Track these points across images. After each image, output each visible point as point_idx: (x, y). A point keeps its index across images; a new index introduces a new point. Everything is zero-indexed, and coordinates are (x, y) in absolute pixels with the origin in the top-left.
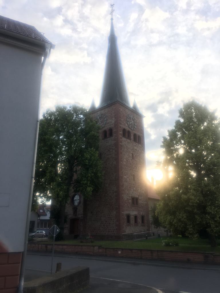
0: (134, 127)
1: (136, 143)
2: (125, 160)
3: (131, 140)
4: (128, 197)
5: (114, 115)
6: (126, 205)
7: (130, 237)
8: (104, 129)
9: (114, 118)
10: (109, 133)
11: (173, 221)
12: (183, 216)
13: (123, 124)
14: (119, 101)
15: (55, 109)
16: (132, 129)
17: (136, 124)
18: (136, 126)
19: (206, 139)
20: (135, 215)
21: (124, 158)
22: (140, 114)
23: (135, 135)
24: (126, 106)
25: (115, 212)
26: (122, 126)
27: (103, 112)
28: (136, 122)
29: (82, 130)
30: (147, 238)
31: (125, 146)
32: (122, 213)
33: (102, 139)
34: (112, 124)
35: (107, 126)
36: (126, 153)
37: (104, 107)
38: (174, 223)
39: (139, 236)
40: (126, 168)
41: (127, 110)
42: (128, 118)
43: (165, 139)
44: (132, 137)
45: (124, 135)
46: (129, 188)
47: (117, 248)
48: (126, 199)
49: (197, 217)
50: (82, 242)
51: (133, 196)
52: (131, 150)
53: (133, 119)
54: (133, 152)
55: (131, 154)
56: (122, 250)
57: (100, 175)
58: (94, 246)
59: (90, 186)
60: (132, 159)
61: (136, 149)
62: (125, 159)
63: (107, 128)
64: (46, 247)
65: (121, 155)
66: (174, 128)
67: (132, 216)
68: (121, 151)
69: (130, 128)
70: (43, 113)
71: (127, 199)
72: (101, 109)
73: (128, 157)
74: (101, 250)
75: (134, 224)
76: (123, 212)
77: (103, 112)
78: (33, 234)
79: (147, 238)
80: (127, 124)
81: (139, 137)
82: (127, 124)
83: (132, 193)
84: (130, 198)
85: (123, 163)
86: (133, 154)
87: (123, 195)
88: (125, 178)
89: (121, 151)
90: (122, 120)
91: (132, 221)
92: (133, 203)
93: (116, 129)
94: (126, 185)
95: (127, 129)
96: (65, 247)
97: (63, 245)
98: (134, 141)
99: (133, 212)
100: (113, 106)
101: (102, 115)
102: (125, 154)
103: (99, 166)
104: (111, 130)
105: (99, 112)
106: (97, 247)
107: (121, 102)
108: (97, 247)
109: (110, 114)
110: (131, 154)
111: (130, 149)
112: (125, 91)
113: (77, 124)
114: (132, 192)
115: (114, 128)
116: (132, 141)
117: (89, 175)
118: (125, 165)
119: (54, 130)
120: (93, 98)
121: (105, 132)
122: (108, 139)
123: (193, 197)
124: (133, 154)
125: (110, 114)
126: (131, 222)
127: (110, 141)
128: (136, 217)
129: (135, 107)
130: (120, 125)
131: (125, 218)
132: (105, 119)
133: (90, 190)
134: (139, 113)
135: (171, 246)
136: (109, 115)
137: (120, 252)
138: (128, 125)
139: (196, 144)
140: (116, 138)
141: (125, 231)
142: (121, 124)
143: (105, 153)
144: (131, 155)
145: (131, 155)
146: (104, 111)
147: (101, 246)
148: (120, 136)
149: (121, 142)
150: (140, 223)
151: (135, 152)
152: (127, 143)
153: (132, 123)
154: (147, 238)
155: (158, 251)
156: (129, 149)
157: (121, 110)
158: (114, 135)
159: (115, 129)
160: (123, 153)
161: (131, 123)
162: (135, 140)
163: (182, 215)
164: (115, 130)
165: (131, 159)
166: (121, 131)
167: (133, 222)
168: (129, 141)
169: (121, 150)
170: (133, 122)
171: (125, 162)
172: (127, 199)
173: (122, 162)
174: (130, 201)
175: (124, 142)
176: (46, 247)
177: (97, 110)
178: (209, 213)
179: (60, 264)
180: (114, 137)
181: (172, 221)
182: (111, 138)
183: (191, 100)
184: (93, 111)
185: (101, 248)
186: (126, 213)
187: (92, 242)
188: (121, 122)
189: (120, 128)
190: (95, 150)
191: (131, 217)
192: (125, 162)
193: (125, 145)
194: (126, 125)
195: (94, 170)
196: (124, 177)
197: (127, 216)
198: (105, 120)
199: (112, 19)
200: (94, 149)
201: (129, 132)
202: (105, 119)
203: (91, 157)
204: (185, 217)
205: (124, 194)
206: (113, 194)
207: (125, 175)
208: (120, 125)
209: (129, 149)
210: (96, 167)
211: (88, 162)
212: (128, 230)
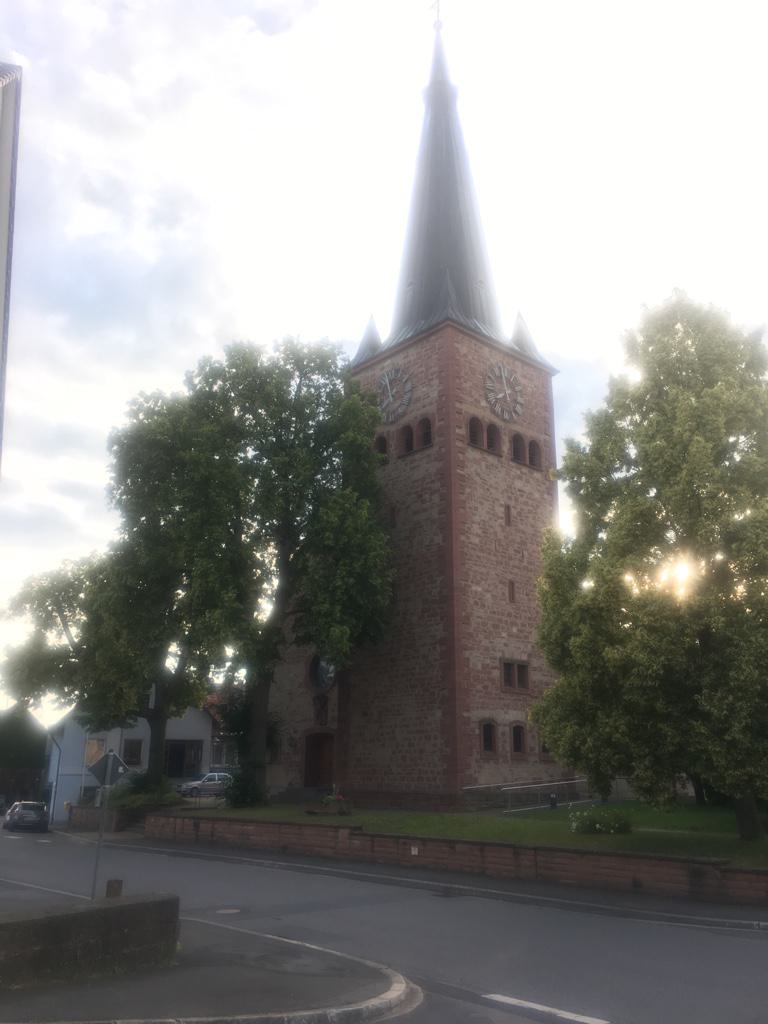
0: (516, 412)
1: (520, 469)
2: (476, 529)
3: (501, 456)
4: (488, 661)
5: (436, 369)
6: (479, 687)
7: (492, 800)
8: (403, 422)
9: (436, 382)
10: (419, 436)
11: (584, 742)
12: (617, 723)
13: (470, 400)
14: (453, 321)
15: (225, 358)
16: (506, 416)
17: (519, 399)
18: (521, 405)
19: (698, 442)
20: (515, 722)
21: (473, 523)
22: (540, 363)
23: (517, 439)
24: (484, 336)
25: (439, 714)
26: (464, 407)
27: (400, 360)
28: (520, 391)
29: (320, 426)
30: (553, 803)
31: (477, 479)
32: (465, 714)
33: (399, 458)
34: (431, 404)
35: (413, 411)
36: (482, 504)
37: (405, 341)
38: (583, 749)
39: (522, 798)
40: (479, 557)
41: (486, 350)
42: (489, 377)
43: (572, 447)
44: (506, 447)
45: (473, 439)
46: (492, 629)
47: (407, 838)
48: (480, 667)
49: (667, 729)
50: (310, 813)
51: (507, 656)
52: (502, 493)
53: (508, 381)
54: (509, 498)
55: (501, 505)
56: (423, 842)
57: (379, 581)
58: (337, 828)
59: (341, 622)
60: (504, 524)
61: (519, 490)
62: (475, 526)
63: (413, 416)
64: (196, 826)
65: (462, 510)
66: (604, 406)
67: (505, 725)
68: (463, 497)
69: (497, 416)
70: (186, 375)
71: (485, 667)
72: (399, 348)
73: (490, 519)
74: (357, 842)
75: (509, 755)
76: (468, 711)
77: (400, 360)
78: (196, 784)
79: (553, 806)
80: (487, 399)
81: (534, 447)
82: (487, 399)
83: (506, 645)
84: (497, 663)
85: (468, 538)
86: (508, 508)
87: (467, 654)
88: (476, 592)
89: (463, 497)
90: (464, 385)
91: (504, 743)
92: (508, 680)
93: (443, 419)
94: (478, 617)
95: (486, 416)
96: (251, 828)
97: (245, 822)
98: (512, 460)
99: (506, 713)
100: (433, 338)
101: (397, 371)
102: (476, 509)
103: (375, 550)
104: (426, 423)
105: (389, 362)
106: (347, 831)
107: (464, 323)
108: (347, 831)
109: (424, 369)
110: (501, 505)
111: (496, 488)
112: (481, 282)
113: (301, 408)
114: (504, 641)
115: (436, 416)
116: (503, 459)
117: (340, 583)
118: (476, 545)
119: (218, 429)
120: (519, 315)
121: (407, 431)
122: (417, 456)
123: (642, 657)
124: (508, 508)
125: (424, 369)
126: (500, 749)
127: (424, 465)
128: (518, 731)
129: (520, 340)
130: (458, 405)
131: (477, 731)
132: (409, 386)
133: (342, 637)
134: (535, 361)
135: (600, 832)
136: (420, 370)
137: (414, 851)
138: (489, 402)
139: (669, 463)
140: (443, 450)
141: (476, 781)
142: (461, 402)
143: (408, 507)
144: (502, 509)
145: (500, 511)
146: (405, 358)
147: (360, 828)
148: (459, 444)
149: (463, 466)
150: (537, 751)
151: (516, 500)
152: (487, 467)
153: (505, 397)
154: (553, 806)
155: (536, 849)
156: (493, 491)
157: (463, 350)
158: (437, 440)
159: (439, 421)
160: (468, 505)
161: (500, 396)
162: (517, 456)
163: (616, 721)
164: (442, 423)
165: (501, 526)
166: (460, 428)
167: (508, 749)
168: (491, 459)
169: (462, 493)
170: (508, 392)
171: (477, 535)
172: (485, 667)
173: (463, 538)
174: (496, 674)
175: (474, 464)
176: (196, 826)
177: (385, 352)
178: (706, 717)
179: (119, 883)
180: (436, 448)
181: (578, 743)
182: (427, 452)
183: (674, 299)
184: (372, 357)
185: (356, 835)
186: (477, 714)
187: (342, 813)
188: (461, 395)
189: (457, 416)
190: (356, 494)
191: (500, 730)
192: (477, 535)
193: (478, 474)
194: (483, 403)
195: (356, 566)
196: (474, 588)
197: (485, 726)
198: (406, 390)
199: (438, 26)
200: (354, 490)
201: (493, 431)
202: (409, 386)
203: (343, 519)
204: (623, 728)
205: (472, 649)
206: (435, 648)
207: (478, 584)
208: (458, 405)
209: (493, 491)
210: (364, 557)
211: (332, 537)
212: (488, 776)
